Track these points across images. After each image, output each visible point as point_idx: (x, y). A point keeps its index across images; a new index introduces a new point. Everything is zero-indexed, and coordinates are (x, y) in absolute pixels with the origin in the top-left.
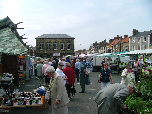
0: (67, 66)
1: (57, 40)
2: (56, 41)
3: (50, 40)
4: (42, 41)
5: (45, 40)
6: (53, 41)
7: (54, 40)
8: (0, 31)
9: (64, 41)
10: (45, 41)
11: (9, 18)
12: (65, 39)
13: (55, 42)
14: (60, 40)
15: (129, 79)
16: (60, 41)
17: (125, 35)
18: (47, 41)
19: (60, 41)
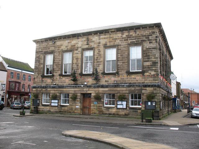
0: (37, 95)
1: (95, 38)
2: (92, 45)
3: (74, 42)
4: (52, 49)
5: (58, 43)
6: (82, 45)
7: (84, 39)
8: (197, 129)
9: (118, 42)
10: (59, 47)
11: (18, 61)
12: (119, 35)
13: (86, 46)
14: (102, 36)
15: (159, 135)
16: (103, 42)
17: (162, 24)
18: (63, 48)
19: (104, 43)
